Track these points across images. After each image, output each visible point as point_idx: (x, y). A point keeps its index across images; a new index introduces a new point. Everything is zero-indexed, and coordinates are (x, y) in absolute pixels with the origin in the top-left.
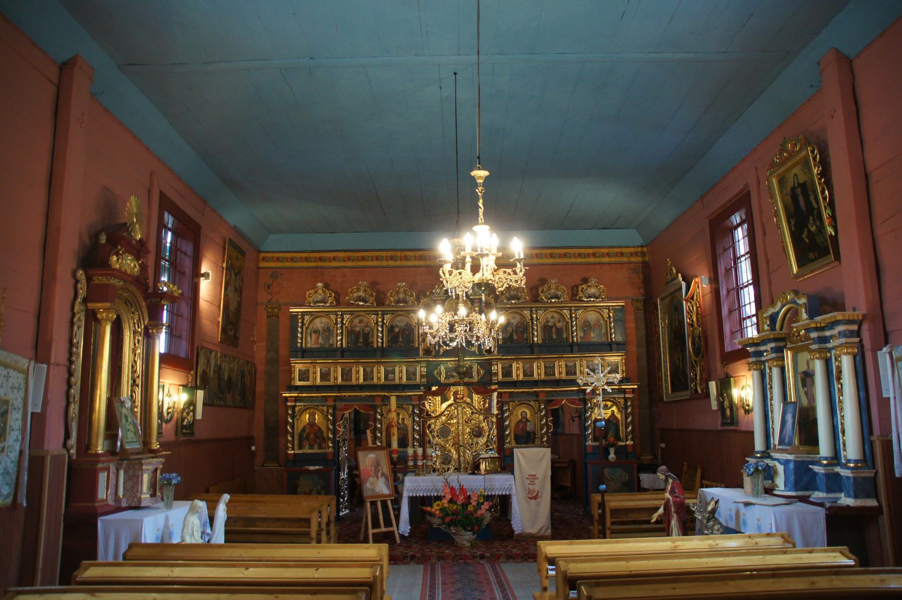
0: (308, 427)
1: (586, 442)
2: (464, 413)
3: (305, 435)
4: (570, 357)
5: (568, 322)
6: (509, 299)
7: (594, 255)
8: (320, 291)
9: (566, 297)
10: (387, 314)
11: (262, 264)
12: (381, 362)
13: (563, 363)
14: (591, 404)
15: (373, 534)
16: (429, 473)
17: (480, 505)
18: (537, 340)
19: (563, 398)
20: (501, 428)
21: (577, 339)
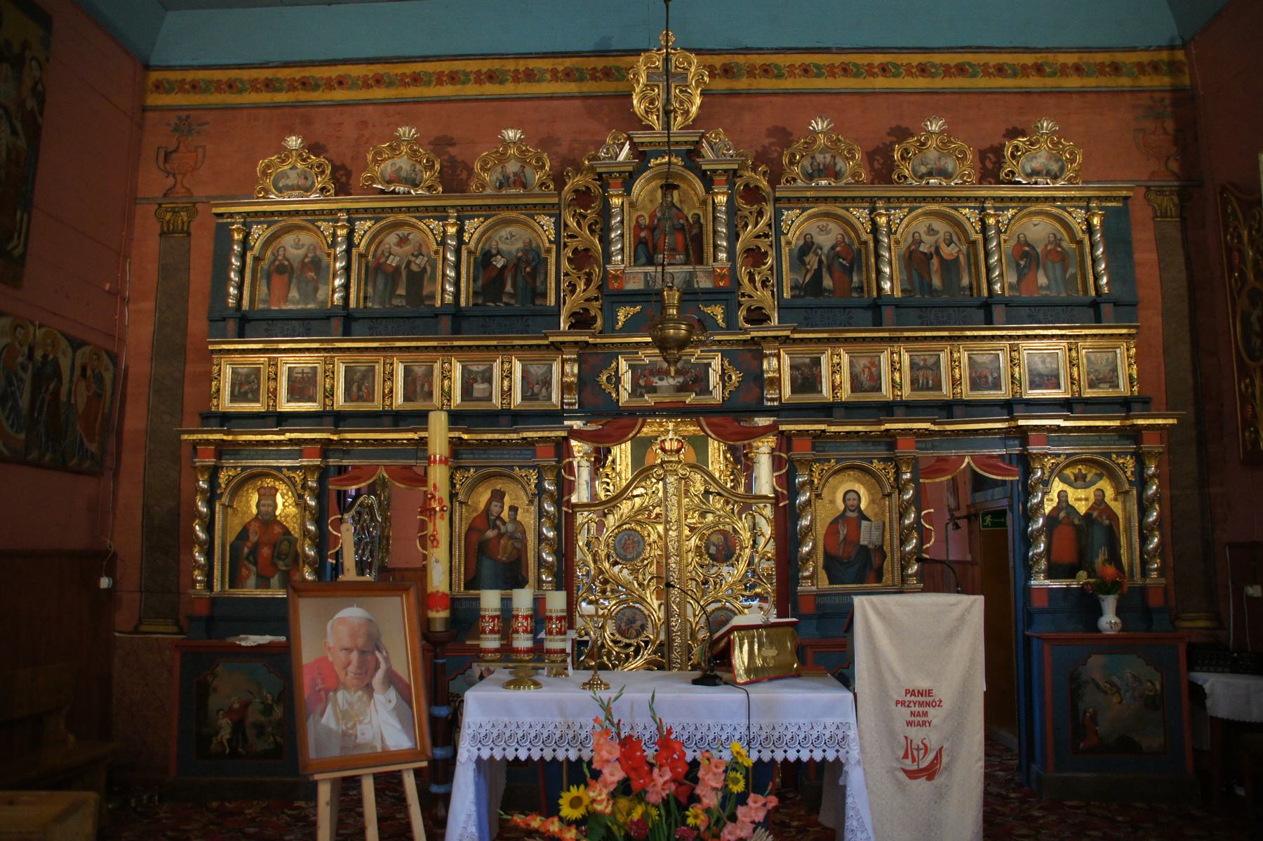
0: (255, 527)
1: (1029, 578)
3: (246, 550)
4: (984, 337)
5: (974, 243)
6: (810, 177)
7: (1039, 69)
9: (968, 170)
10: (472, 217)
12: (453, 347)
14: (1043, 473)
17: (731, 802)
18: (892, 289)
19: (962, 452)
21: (1002, 288)
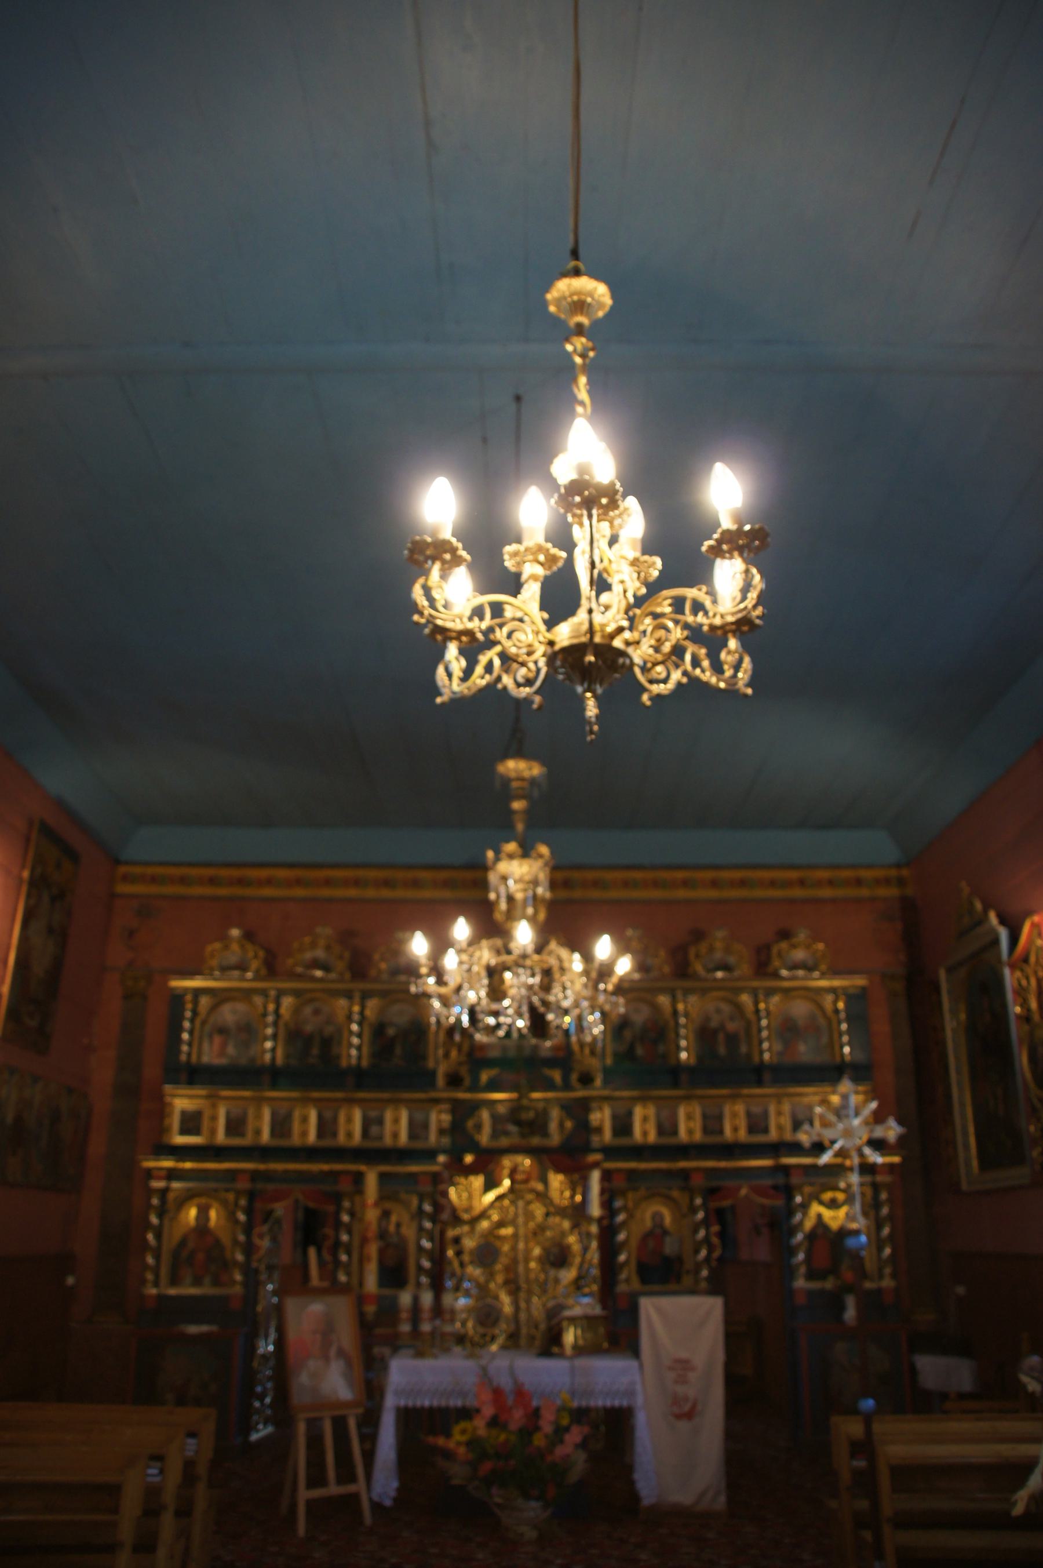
2: (529, 1216)
7: (802, 883)
8: (235, 947)
9: (745, 969)
11: (122, 888)
13: (740, 1108)
15: (310, 1504)
16: (447, 1350)
17: (560, 1432)
20: (609, 1248)
